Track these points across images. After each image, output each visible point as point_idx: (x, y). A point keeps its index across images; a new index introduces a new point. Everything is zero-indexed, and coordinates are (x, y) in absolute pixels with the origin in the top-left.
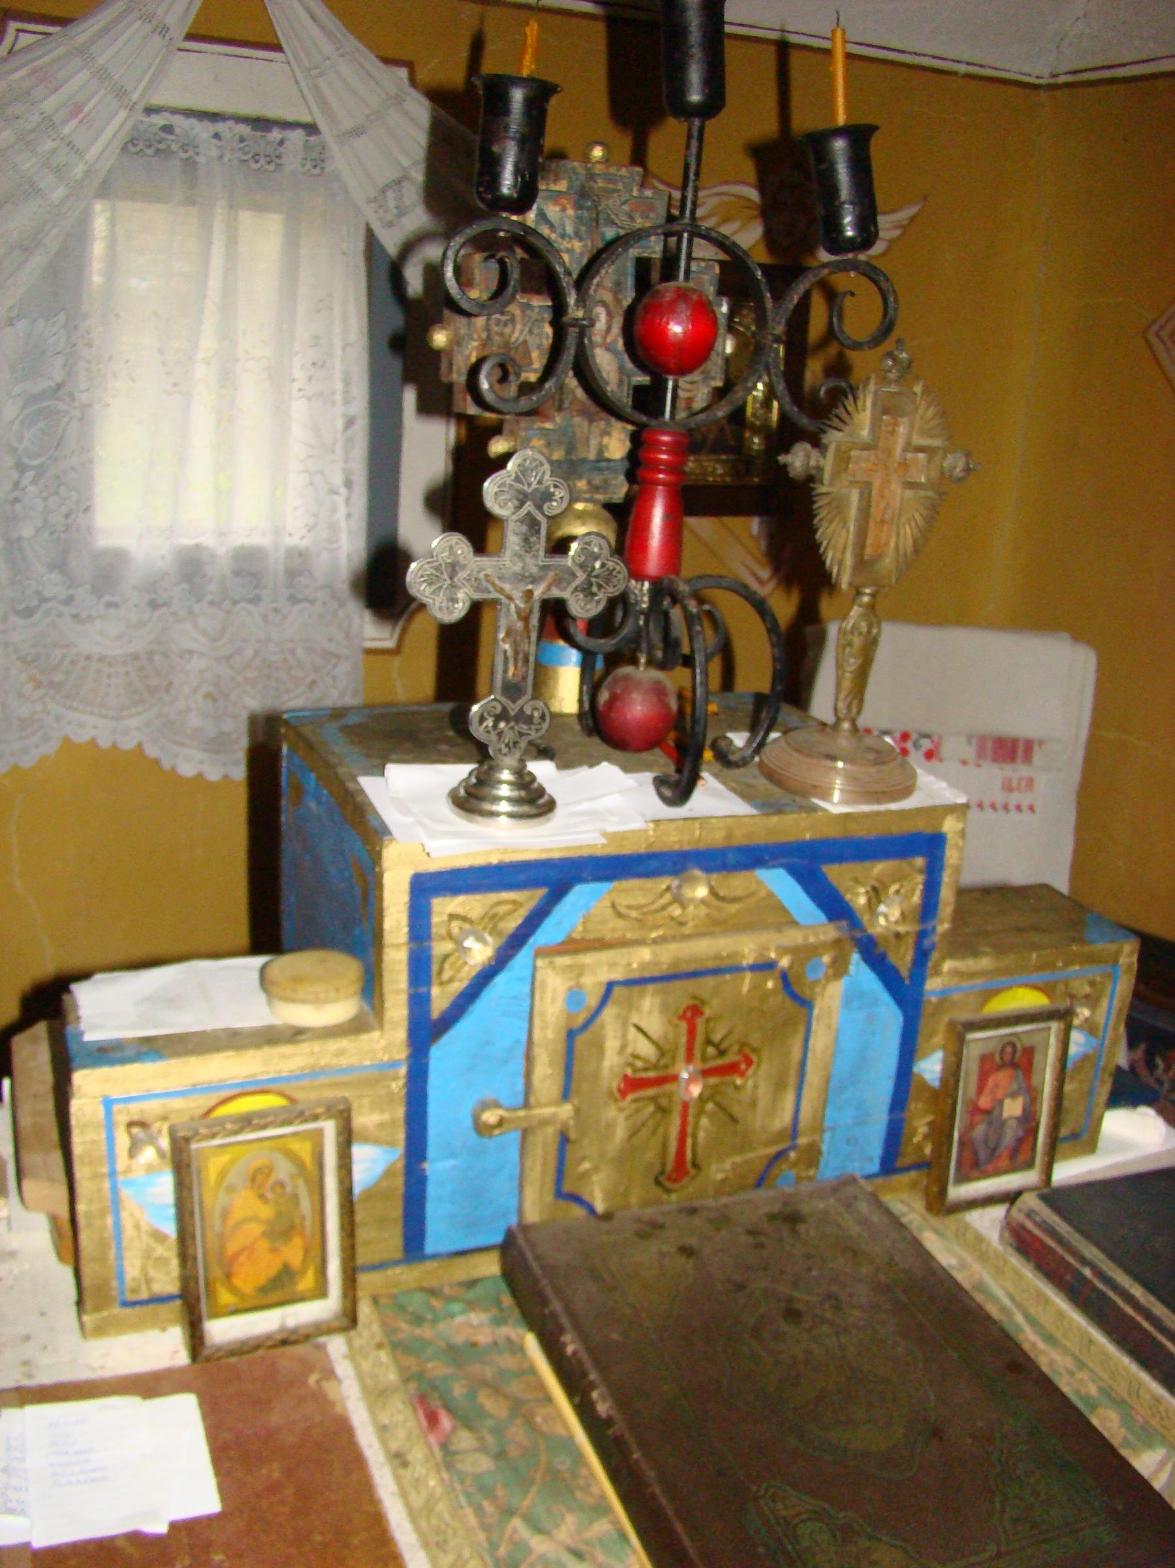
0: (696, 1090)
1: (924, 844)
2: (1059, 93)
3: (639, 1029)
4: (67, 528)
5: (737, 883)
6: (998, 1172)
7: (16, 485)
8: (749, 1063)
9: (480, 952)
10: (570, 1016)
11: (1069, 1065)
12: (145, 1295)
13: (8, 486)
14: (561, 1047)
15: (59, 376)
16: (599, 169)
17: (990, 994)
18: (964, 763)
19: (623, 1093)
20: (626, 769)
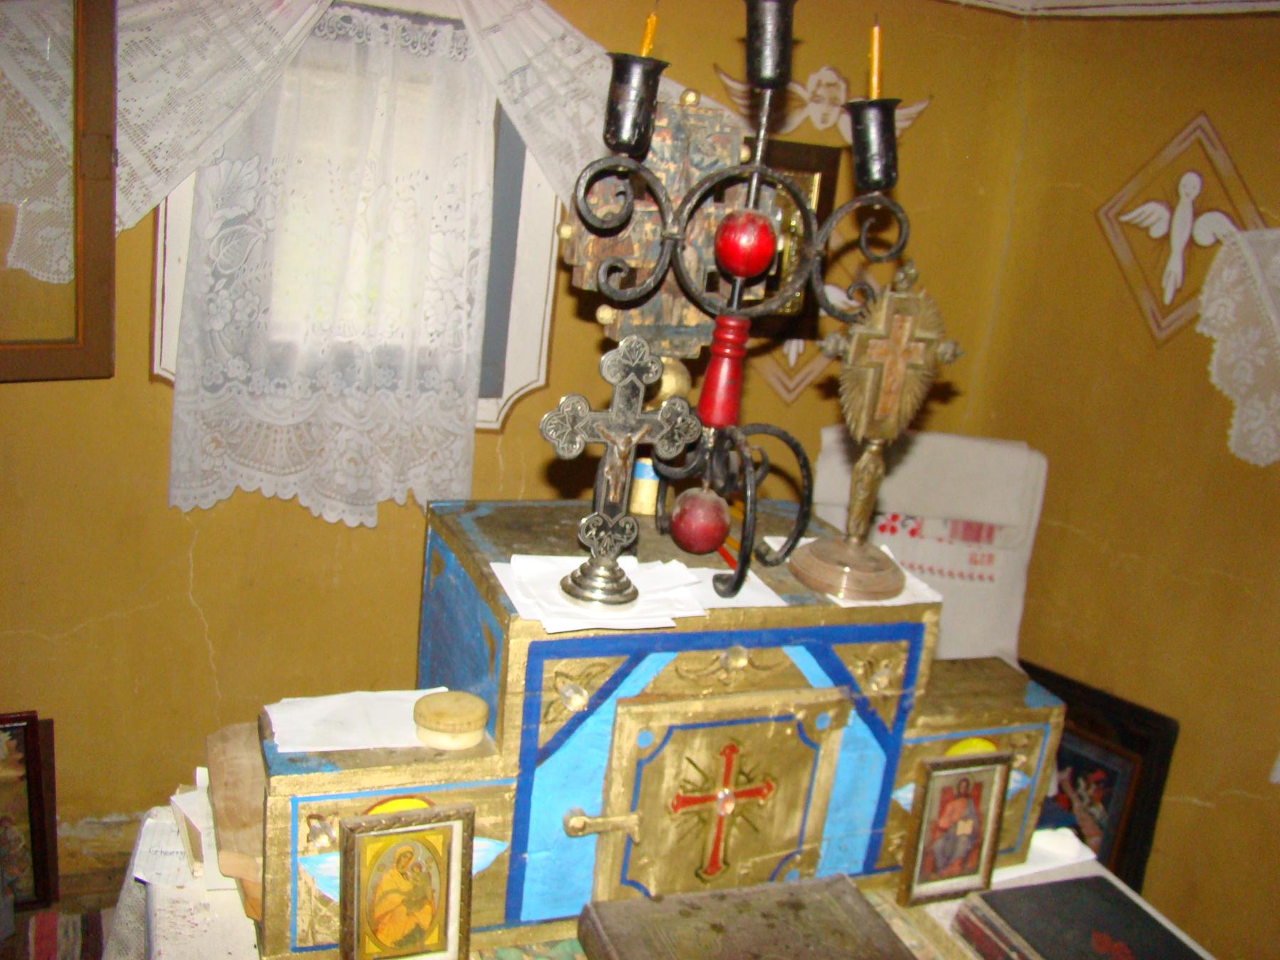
0: (730, 807)
1: (906, 630)
2: (1037, 23)
3: (690, 761)
4: (250, 324)
5: (768, 656)
6: (951, 876)
7: (212, 289)
8: (770, 788)
9: (578, 702)
10: (640, 750)
11: (1009, 797)
12: (311, 944)
13: (206, 289)
14: (632, 774)
15: (250, 205)
16: (691, 111)
17: (952, 742)
18: (940, 540)
19: (676, 808)
20: (689, 565)
